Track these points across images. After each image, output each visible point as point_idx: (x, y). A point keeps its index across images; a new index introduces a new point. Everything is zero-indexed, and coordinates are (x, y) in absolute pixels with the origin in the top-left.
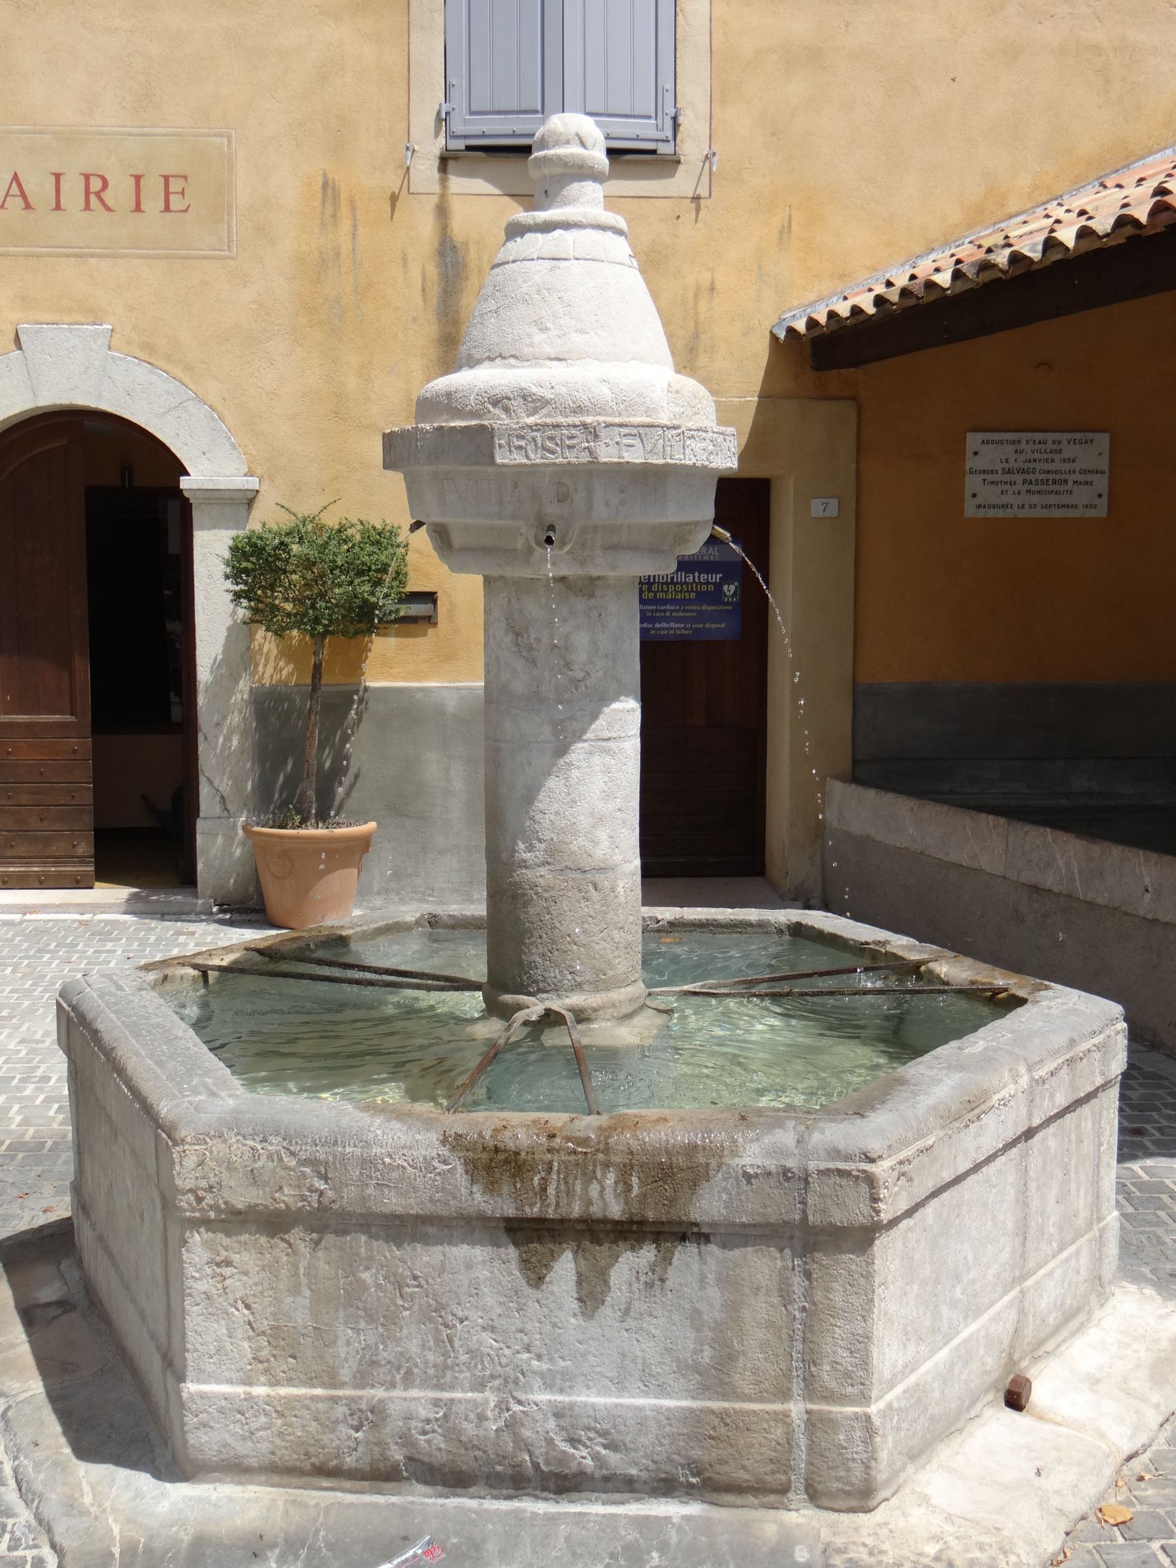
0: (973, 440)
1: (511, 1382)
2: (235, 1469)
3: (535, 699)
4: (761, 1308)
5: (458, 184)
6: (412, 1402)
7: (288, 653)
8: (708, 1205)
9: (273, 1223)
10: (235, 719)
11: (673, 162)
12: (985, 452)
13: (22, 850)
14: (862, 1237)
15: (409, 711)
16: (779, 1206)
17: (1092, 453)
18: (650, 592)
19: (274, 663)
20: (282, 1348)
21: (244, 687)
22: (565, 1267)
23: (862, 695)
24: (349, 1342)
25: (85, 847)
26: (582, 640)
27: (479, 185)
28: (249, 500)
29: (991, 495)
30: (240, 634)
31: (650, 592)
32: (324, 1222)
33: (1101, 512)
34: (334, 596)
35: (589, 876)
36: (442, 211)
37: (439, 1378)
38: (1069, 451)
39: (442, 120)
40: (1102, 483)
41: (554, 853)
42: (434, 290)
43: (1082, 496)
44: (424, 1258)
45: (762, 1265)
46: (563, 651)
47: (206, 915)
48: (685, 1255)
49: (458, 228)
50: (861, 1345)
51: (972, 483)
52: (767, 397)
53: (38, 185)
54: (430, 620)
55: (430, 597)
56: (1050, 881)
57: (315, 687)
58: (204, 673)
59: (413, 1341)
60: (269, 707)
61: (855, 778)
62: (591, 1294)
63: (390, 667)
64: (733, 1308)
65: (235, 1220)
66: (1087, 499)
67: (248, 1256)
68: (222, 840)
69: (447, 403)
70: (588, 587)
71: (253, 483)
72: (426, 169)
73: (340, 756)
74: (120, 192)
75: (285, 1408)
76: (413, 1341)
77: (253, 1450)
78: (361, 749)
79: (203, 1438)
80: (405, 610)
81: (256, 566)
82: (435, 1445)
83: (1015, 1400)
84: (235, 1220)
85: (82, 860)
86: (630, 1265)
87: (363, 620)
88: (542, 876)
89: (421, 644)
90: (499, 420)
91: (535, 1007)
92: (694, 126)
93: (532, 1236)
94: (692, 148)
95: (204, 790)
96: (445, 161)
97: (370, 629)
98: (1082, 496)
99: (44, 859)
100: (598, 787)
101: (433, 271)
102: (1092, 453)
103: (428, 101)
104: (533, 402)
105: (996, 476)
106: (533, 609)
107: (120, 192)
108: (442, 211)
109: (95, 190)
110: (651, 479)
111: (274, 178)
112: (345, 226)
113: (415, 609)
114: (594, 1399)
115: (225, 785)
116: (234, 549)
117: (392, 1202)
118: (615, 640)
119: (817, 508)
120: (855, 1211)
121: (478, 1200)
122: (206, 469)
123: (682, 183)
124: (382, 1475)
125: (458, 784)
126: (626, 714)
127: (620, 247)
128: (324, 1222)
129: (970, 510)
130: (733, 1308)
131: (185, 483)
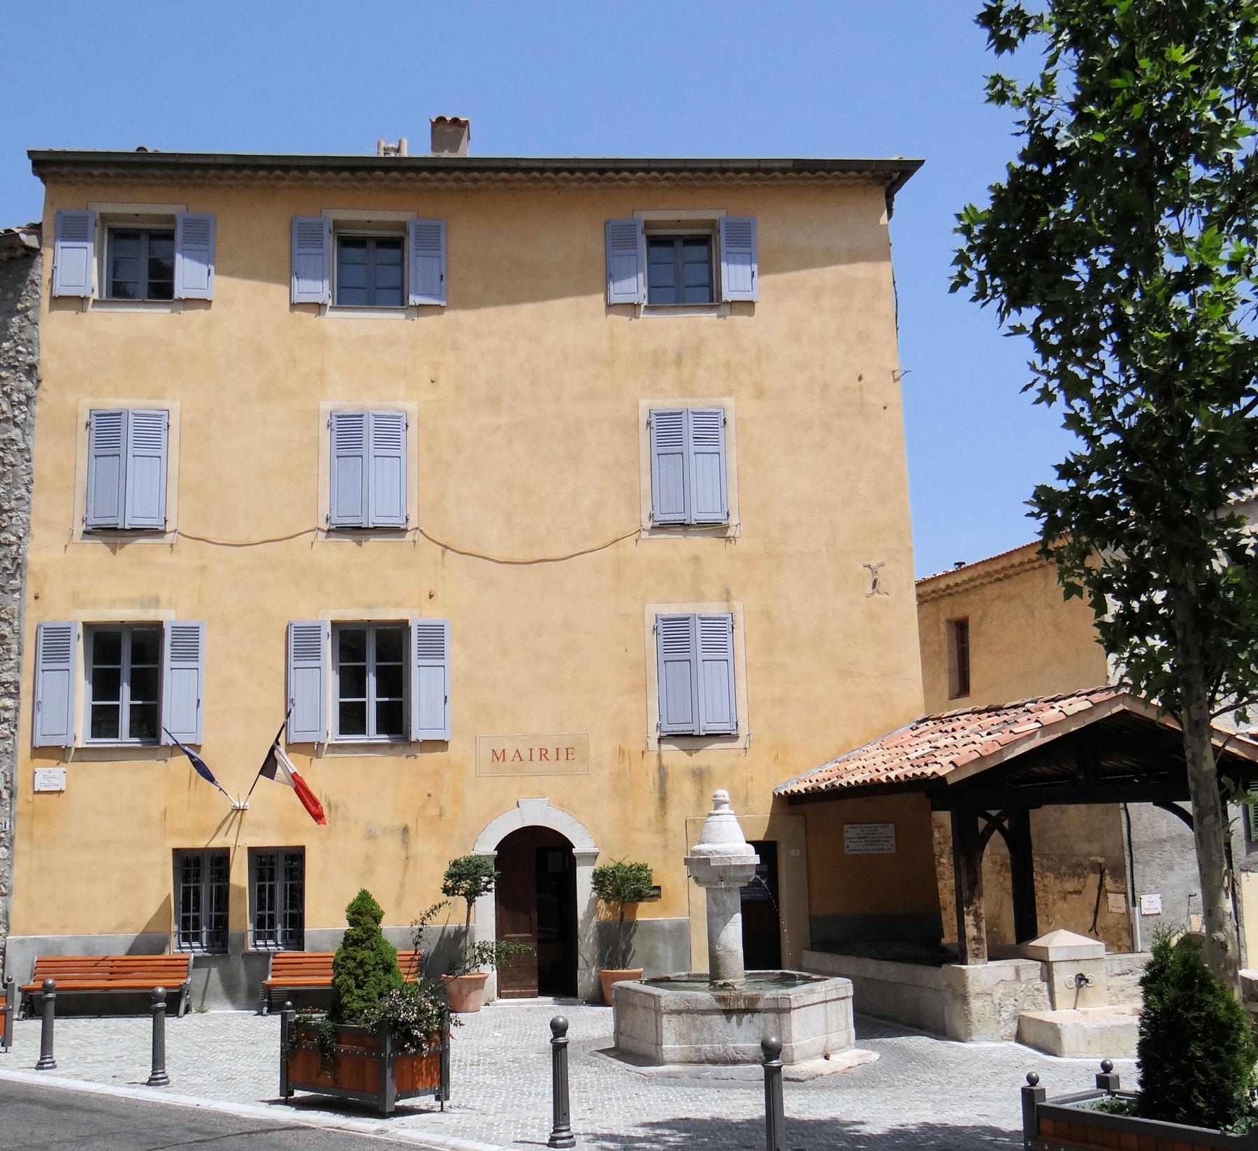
0: (846, 827)
1: (725, 1042)
2: (673, 1062)
3: (719, 914)
4: (771, 1026)
5: (664, 747)
6: (707, 1047)
7: (609, 909)
8: (760, 1005)
9: (679, 1012)
10: (591, 932)
11: (736, 737)
12: (851, 832)
13: (513, 984)
14: (789, 1010)
15: (652, 929)
16: (772, 1005)
17: (889, 830)
18: (743, 890)
19: (604, 913)
20: (681, 1037)
21: (595, 920)
22: (734, 1018)
23: (813, 919)
24: (694, 1036)
25: (535, 983)
26: (729, 902)
27: (672, 747)
28: (596, 856)
29: (853, 846)
30: (593, 902)
31: (743, 890)
32: (688, 1011)
33: (894, 850)
34: (627, 887)
35: (732, 953)
36: (659, 756)
37: (712, 1042)
38: (880, 830)
39: (658, 727)
40: (893, 841)
41: (725, 947)
42: (658, 783)
43: (886, 846)
44: (708, 1018)
45: (771, 1016)
46: (724, 903)
47: (581, 1004)
48: (756, 1015)
49: (665, 762)
50: (790, 1032)
51: (847, 842)
52: (773, 815)
53: (525, 753)
54: (659, 896)
55: (658, 888)
56: (868, 976)
57: (622, 920)
58: (580, 916)
59: (706, 1035)
60: (603, 928)
61: (813, 948)
62: (739, 1023)
63: (645, 913)
64: (766, 1025)
65: (672, 1012)
66: (889, 847)
67: (674, 1018)
68: (586, 978)
69: (699, 852)
70: (728, 890)
71: (596, 850)
72: (653, 743)
73: (629, 946)
74: (552, 754)
75: (682, 1050)
76: (706, 1035)
77: (676, 1058)
78: (635, 942)
79: (667, 1057)
80: (652, 893)
81: (600, 879)
82: (711, 1056)
83: (827, 1058)
84: (672, 1012)
85: (533, 987)
86: (747, 1017)
87: (639, 896)
88: (722, 953)
89: (655, 905)
90: (711, 857)
91: (721, 982)
92: (743, 725)
93: (728, 1013)
94: (743, 732)
95: (580, 958)
96: (660, 740)
97: (641, 900)
98: (886, 846)
99: (519, 987)
100: (733, 934)
101: (657, 776)
102: (889, 830)
103: (654, 720)
104: (718, 853)
105: (854, 839)
106: (718, 895)
107: (552, 754)
108: (659, 756)
109: (543, 754)
110: (742, 867)
111: (603, 748)
112: (627, 762)
113: (656, 892)
114: (740, 1045)
115: (588, 956)
116: (595, 874)
117: (702, 1007)
118: (735, 901)
119: (793, 852)
120: (786, 1005)
121: (717, 1005)
122: (581, 845)
123: (740, 743)
124: (701, 1062)
125: (670, 955)
126: (738, 917)
127: (733, 818)
128: (688, 1011)
129: (847, 852)
130: (766, 1025)
131: (574, 851)
